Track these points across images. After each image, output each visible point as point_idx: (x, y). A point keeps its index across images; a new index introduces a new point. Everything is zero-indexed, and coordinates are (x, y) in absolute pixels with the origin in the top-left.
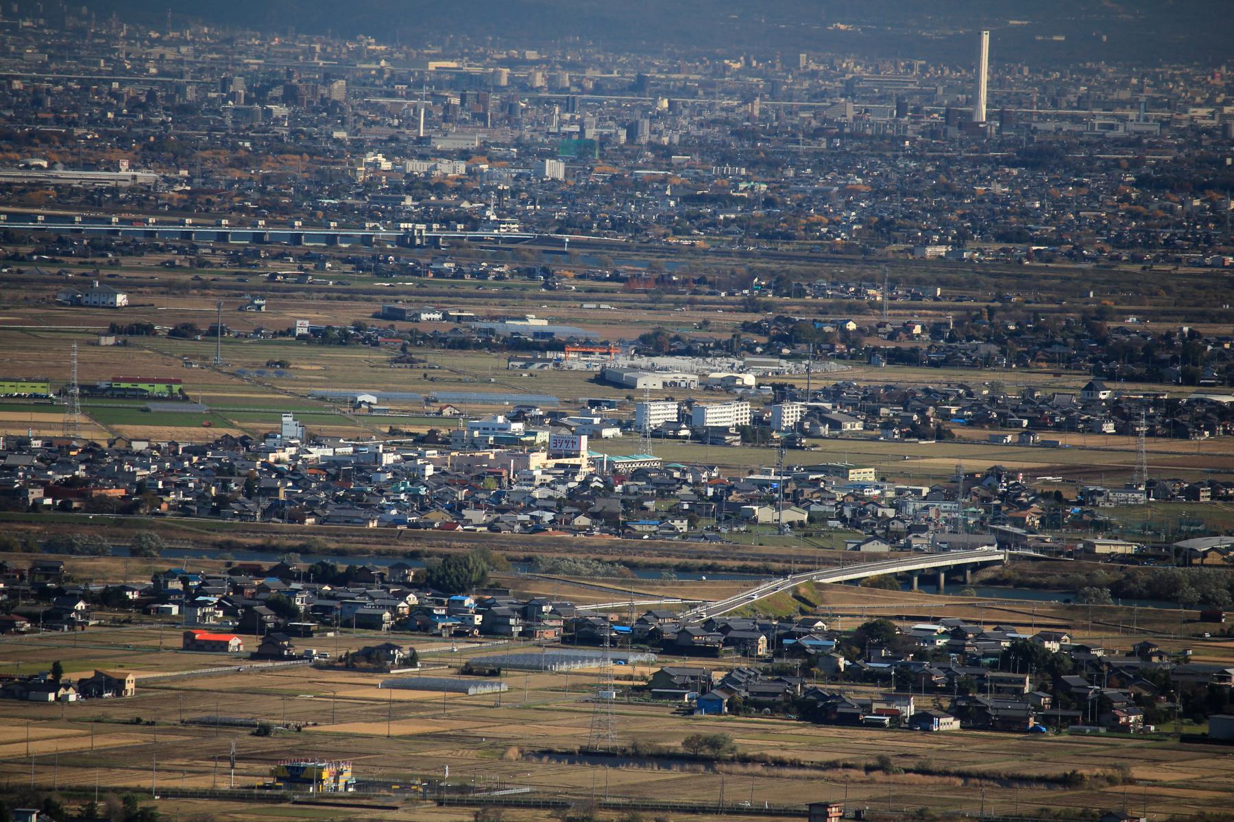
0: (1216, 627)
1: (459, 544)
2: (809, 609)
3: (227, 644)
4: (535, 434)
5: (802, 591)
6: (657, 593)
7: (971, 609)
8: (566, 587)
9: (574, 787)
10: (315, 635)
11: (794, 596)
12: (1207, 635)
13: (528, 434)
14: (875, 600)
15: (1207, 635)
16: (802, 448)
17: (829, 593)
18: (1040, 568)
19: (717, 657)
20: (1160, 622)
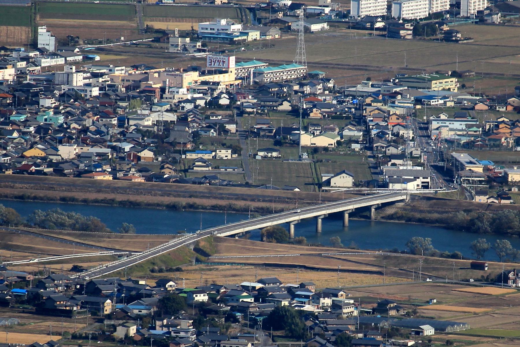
0: (479, 273)
1: (20, 185)
2: (203, 258)
3: (317, 75)
4: (247, 34)
5: (202, 244)
6: (102, 245)
7: (318, 259)
8: (39, 239)
9: (371, 291)
10: (59, 198)
11: (195, 249)
12: (472, 280)
13: (242, 34)
14: (253, 251)
15: (472, 280)
16: (457, 41)
17: (223, 245)
18: (431, 206)
19: (71, 317)
20: (443, 269)
